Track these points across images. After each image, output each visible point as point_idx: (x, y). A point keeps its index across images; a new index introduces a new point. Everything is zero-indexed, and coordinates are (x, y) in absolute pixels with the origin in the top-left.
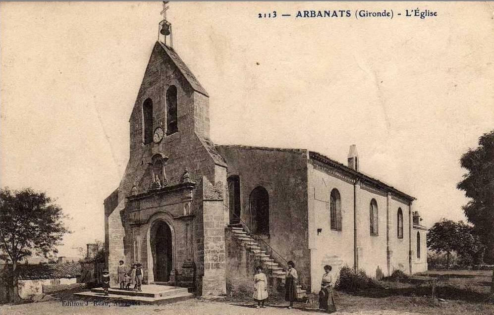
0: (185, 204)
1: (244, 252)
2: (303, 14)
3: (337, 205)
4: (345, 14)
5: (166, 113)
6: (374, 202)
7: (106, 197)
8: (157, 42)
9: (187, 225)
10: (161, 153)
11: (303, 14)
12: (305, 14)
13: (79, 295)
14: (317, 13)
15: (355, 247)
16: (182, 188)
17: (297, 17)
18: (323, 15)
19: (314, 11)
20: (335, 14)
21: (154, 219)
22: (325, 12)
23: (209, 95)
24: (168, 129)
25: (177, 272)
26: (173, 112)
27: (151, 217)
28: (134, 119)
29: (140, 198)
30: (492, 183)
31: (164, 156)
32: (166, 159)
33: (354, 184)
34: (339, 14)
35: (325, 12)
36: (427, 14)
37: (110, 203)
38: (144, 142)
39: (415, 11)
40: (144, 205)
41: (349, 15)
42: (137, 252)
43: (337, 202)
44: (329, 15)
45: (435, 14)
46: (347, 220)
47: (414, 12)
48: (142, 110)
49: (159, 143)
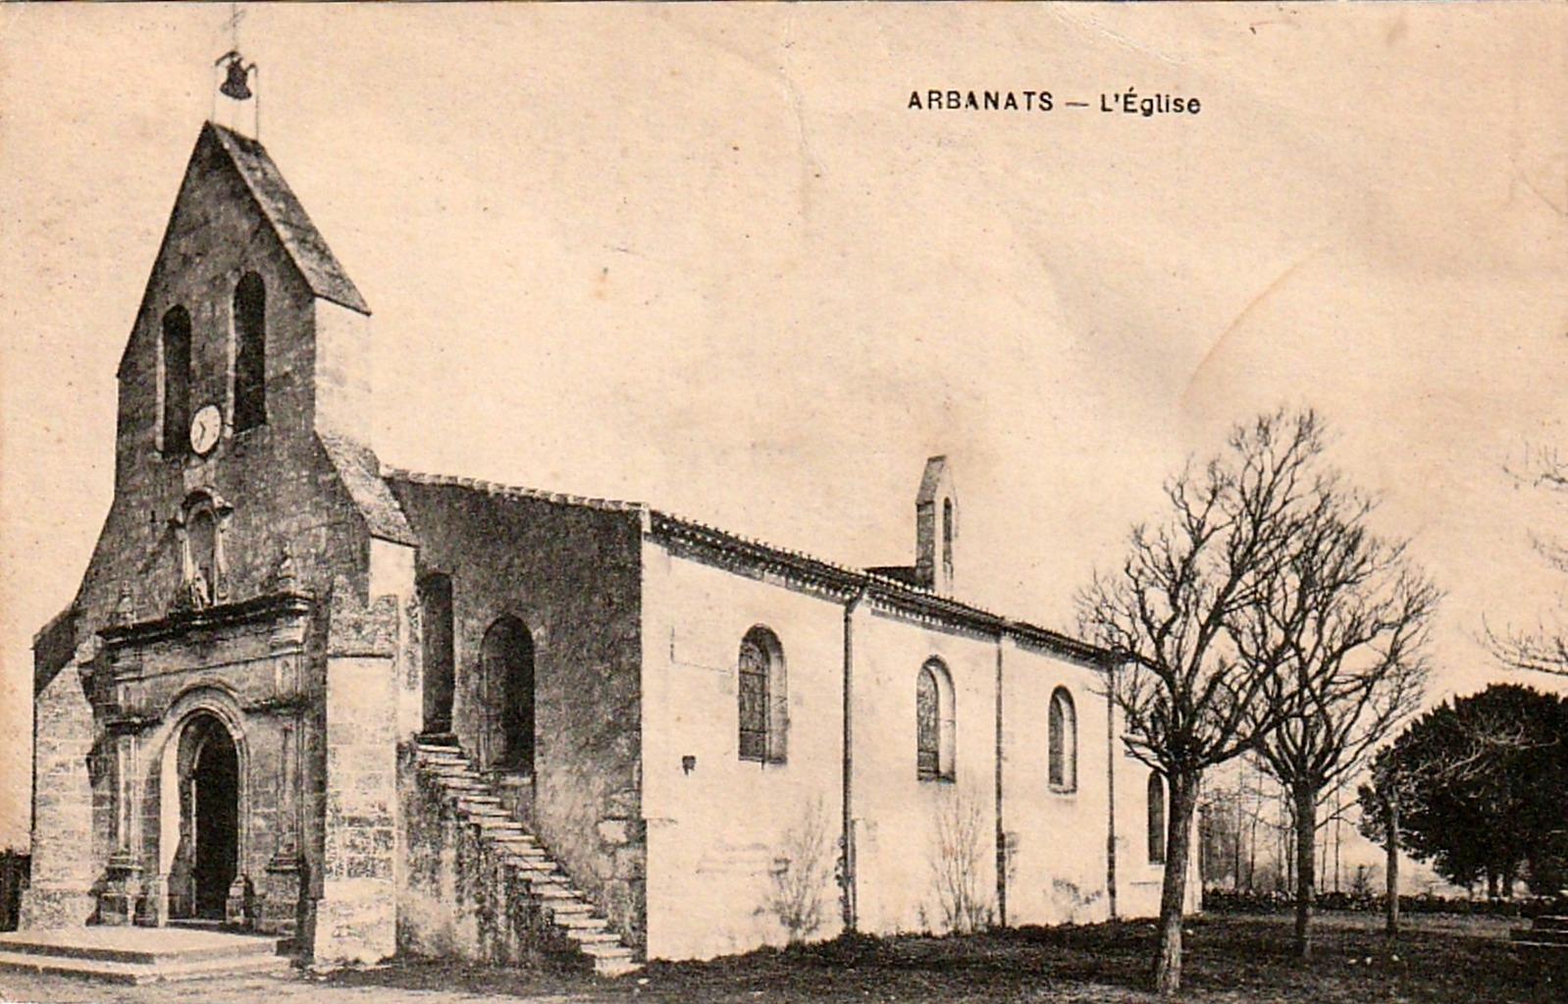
0: (279, 662)
1: (449, 824)
2: (924, 100)
3: (774, 678)
4: (1036, 100)
5: (232, 361)
9: (286, 732)
10: (209, 490)
15: (845, 818)
16: (266, 610)
18: (924, 102)
19: (956, 93)
22: (987, 95)
23: (370, 307)
24: (236, 412)
26: (252, 356)
27: (1357, 753)
28: (129, 370)
29: (141, 637)
31: (218, 500)
32: (225, 511)
33: (850, 605)
34: (1021, 100)
35: (987, 95)
37: (53, 648)
38: (161, 448)
40: (155, 661)
41: (1046, 105)
42: (127, 818)
43: (775, 666)
44: (996, 105)
48: (160, 342)
49: (204, 457)
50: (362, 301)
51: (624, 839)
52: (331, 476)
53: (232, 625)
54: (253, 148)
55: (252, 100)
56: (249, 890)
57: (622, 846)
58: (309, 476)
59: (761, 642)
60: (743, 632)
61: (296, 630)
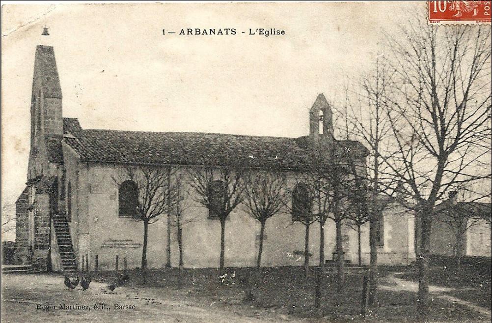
2: (186, 32)
11: (186, 32)
12: (188, 32)
14: (216, 32)
17: (180, 34)
20: (220, 32)
22: (211, 30)
30: (464, 2)
36: (273, 33)
39: (260, 29)
45: (250, 29)
47: (259, 30)
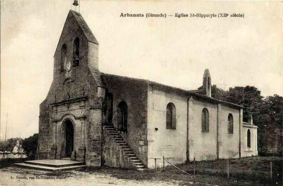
6: (230, 117)
7: (40, 103)
8: (70, 10)
9: (82, 123)
13: (18, 165)
21: (64, 118)
25: (76, 152)
27: (63, 117)
46: (181, 123)
50: (97, 42)
51: (144, 144)
52: (91, 75)
53: (73, 103)
54: (78, 15)
55: (79, 6)
56: (75, 153)
57: (143, 145)
58: (87, 75)
59: (170, 106)
60: (167, 104)
61: (74, 158)
